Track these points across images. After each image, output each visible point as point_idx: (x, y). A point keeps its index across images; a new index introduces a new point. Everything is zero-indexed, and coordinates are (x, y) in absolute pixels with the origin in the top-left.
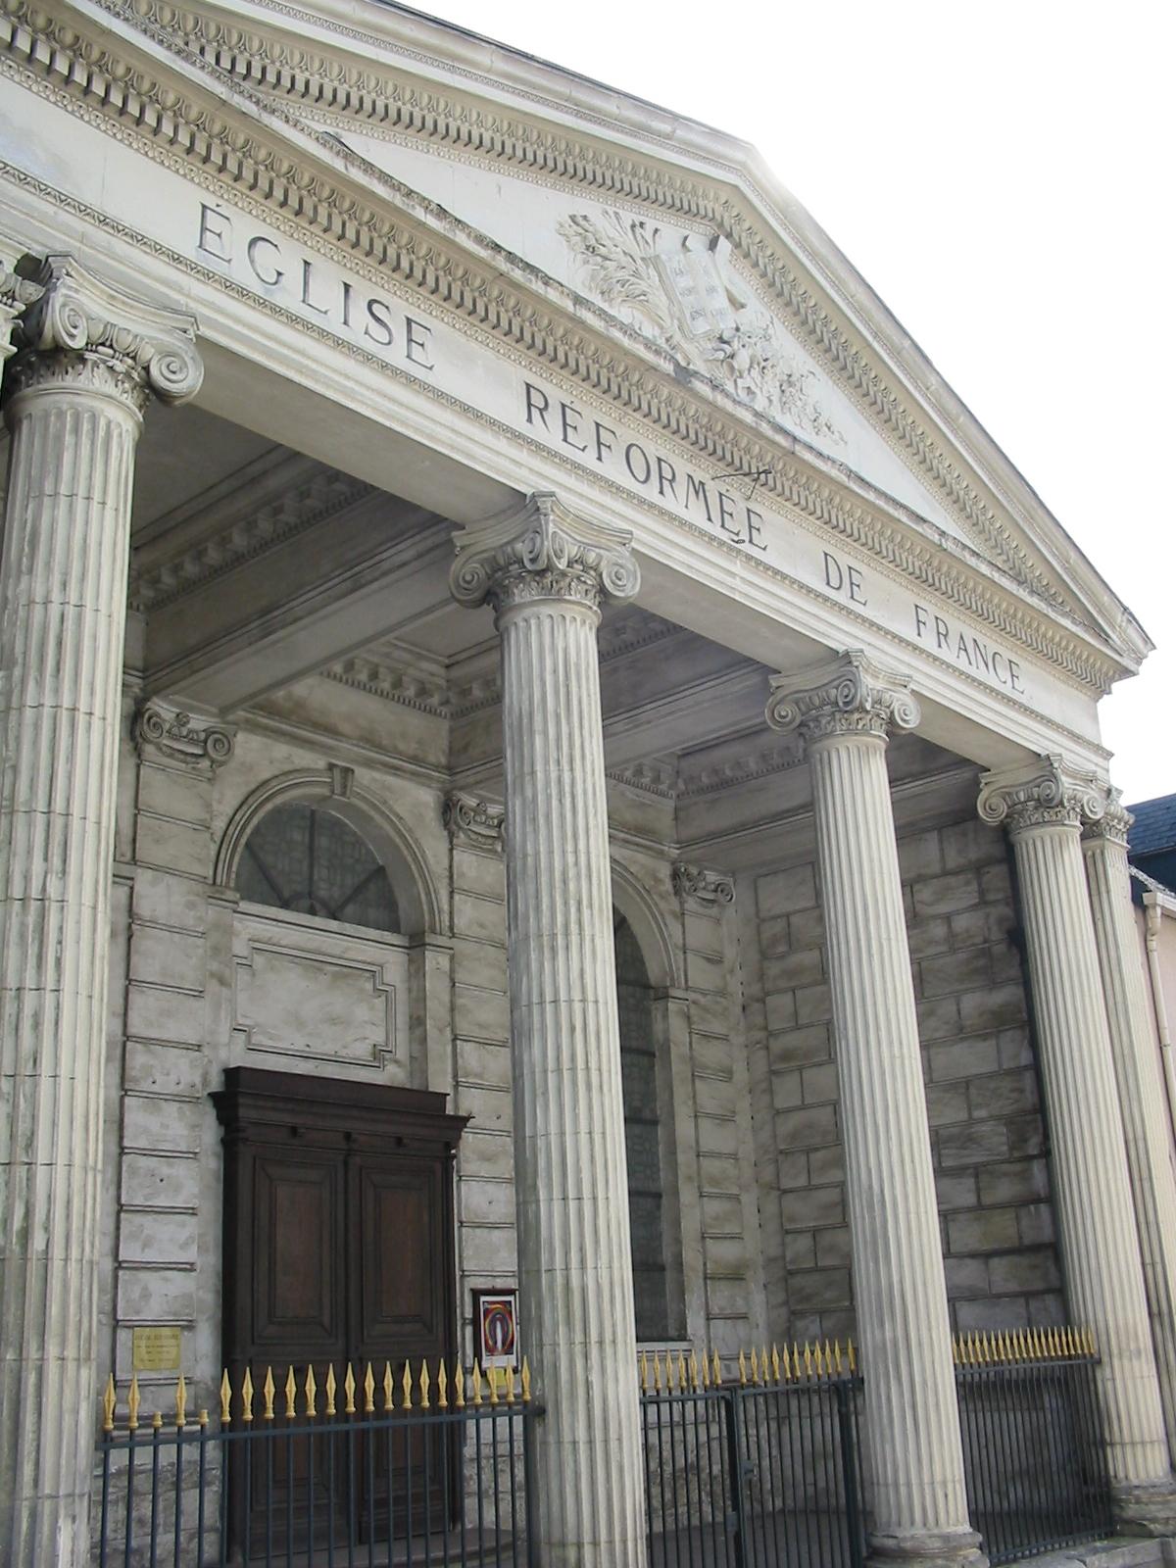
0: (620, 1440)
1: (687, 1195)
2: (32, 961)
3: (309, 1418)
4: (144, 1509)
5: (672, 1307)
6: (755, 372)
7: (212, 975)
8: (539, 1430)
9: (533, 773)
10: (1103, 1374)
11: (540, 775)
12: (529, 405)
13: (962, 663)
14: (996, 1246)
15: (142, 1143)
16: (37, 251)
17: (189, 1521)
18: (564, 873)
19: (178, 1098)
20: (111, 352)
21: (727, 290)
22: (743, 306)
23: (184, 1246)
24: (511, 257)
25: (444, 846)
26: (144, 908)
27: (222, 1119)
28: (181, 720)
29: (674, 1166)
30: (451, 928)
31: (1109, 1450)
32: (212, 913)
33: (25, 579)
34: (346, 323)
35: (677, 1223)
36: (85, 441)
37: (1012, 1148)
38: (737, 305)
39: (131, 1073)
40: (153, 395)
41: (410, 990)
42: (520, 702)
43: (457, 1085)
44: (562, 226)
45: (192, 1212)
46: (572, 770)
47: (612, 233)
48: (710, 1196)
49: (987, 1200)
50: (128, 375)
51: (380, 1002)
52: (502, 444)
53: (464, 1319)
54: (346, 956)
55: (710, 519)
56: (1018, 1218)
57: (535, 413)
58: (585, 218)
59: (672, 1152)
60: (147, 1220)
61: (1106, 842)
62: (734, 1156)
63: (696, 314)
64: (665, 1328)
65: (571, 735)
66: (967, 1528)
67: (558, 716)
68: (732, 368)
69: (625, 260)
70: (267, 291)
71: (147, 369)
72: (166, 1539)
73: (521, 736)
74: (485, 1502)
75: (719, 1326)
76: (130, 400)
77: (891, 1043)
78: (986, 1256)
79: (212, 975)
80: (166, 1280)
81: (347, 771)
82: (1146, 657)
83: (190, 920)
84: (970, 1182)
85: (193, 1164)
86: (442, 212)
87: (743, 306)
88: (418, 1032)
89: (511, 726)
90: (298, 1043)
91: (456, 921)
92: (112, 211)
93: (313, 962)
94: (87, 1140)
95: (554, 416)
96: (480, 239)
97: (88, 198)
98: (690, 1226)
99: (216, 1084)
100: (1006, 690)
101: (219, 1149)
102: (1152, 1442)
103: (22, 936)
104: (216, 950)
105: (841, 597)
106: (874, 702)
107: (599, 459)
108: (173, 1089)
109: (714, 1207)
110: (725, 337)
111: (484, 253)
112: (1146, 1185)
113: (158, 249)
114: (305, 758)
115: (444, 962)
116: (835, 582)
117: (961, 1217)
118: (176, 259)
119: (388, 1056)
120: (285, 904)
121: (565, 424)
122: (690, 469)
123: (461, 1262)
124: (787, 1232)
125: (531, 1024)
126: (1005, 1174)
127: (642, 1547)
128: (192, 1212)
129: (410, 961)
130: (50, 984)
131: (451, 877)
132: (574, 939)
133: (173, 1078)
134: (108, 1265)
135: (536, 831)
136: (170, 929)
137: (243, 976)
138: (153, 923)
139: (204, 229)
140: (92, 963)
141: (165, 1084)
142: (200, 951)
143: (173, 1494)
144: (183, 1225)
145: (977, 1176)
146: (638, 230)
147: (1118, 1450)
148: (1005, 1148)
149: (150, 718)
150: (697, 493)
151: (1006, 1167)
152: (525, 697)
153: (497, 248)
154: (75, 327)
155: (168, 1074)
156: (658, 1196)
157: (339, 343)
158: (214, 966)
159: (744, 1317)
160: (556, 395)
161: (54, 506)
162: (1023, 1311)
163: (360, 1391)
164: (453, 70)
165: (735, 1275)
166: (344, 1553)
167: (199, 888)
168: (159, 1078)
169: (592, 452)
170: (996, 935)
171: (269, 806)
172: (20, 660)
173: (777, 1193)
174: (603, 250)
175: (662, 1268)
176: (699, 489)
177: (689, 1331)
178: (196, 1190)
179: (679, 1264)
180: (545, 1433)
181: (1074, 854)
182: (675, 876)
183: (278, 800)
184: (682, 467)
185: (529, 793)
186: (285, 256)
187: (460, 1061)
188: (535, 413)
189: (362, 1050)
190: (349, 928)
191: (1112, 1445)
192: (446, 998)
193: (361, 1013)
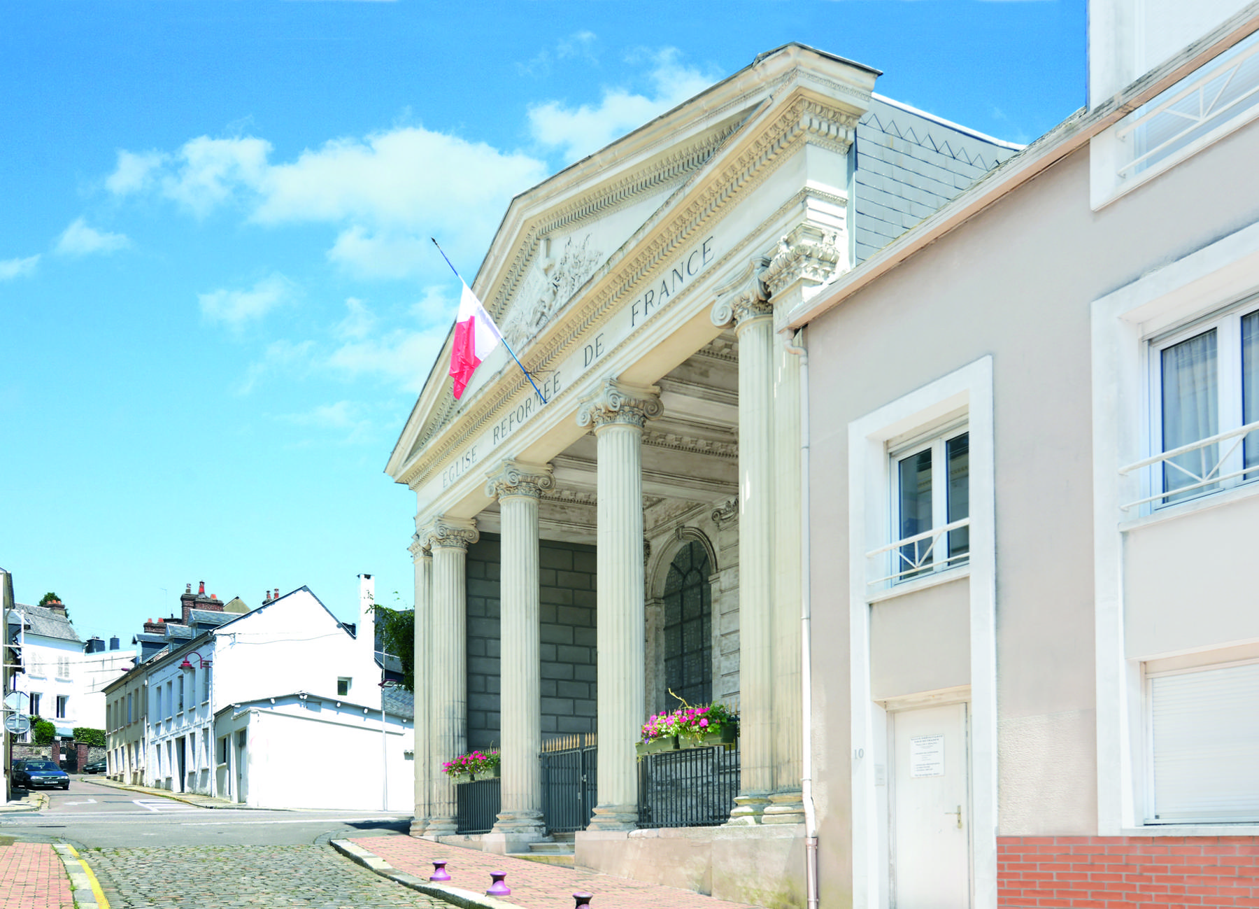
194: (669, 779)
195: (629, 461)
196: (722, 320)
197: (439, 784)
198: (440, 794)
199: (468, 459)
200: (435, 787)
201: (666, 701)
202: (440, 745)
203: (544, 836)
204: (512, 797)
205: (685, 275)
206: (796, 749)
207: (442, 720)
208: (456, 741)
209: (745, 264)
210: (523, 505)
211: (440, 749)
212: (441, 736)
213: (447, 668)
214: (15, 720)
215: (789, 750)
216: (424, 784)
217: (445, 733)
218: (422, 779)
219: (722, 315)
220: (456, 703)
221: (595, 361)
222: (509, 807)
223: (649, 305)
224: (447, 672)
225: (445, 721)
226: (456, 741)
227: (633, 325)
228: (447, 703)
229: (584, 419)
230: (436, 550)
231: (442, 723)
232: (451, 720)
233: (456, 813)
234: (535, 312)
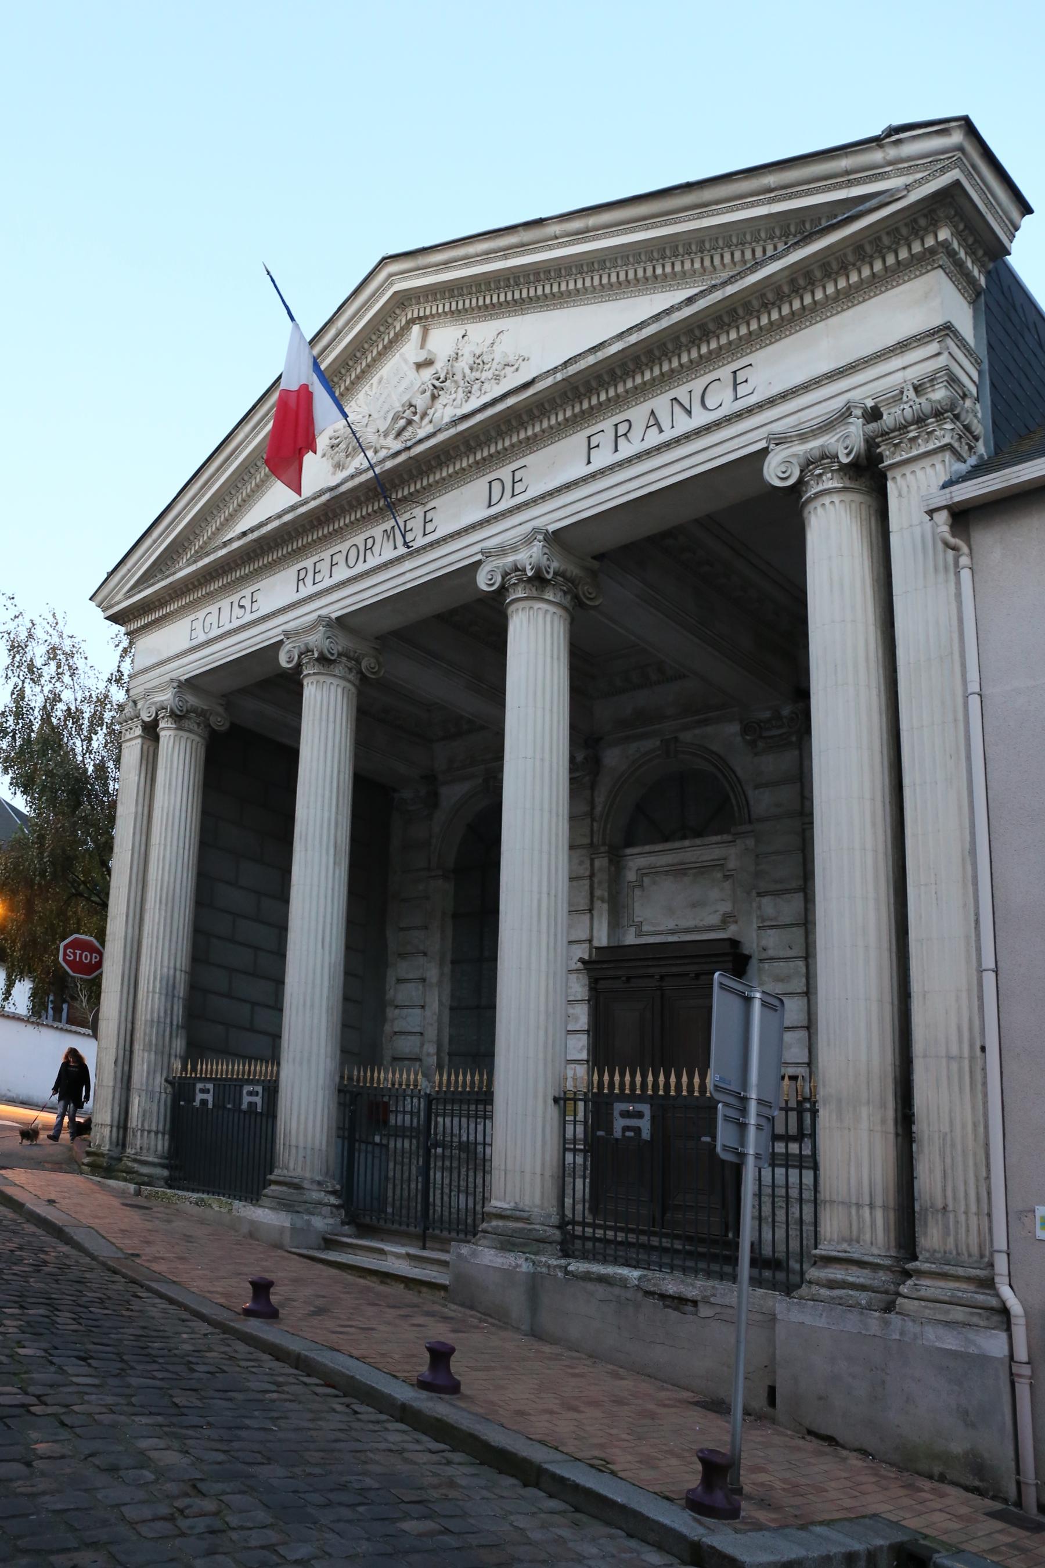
3: (604, 1094)
20: (829, 460)
51: (727, 885)
54: (700, 860)
74: (764, 1226)
90: (671, 924)
91: (137, 778)
93: (679, 871)
120: (666, 840)
124: (569, 1032)
193: (714, 894)
194: (456, 1139)
195: (558, 658)
196: (782, 479)
197: (143, 1099)
198: (144, 1115)
199: (242, 607)
200: (136, 1102)
201: (450, 1022)
202: (151, 1035)
203: (343, 1223)
204: (297, 1153)
205: (696, 408)
206: (962, 1195)
207: (157, 996)
208: (174, 1034)
209: (838, 404)
210: (340, 690)
211: (150, 1041)
212: (152, 1021)
213: (169, 914)
214: (483, 1213)
215: (944, 1190)
216: (114, 1092)
217: (159, 1017)
218: (111, 1084)
219: (784, 472)
220: (178, 973)
221: (507, 503)
222: (291, 1166)
223: (301, 583)
224: (169, 921)
225: (160, 999)
226: (174, 1034)
227: (643, 440)
228: (165, 970)
229: (491, 580)
230: (167, 733)
231: (157, 1000)
232: (170, 998)
233: (166, 1148)
234: (396, 418)
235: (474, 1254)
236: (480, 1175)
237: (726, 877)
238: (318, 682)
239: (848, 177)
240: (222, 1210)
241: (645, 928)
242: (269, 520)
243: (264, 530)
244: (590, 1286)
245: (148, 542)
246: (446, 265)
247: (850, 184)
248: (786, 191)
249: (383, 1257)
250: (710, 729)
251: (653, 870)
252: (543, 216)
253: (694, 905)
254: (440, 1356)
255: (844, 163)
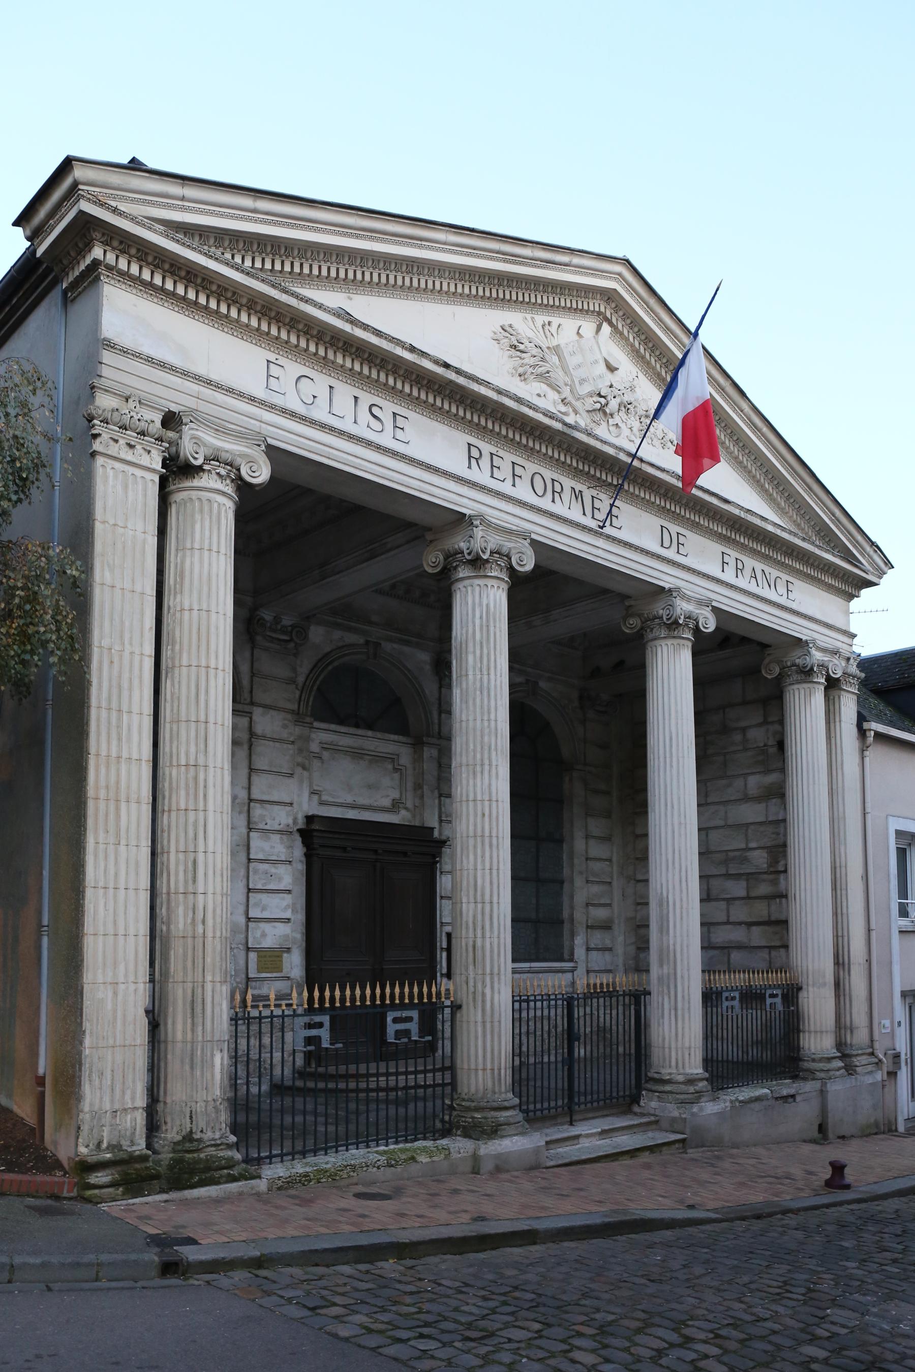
0: (500, 1022)
1: (579, 882)
2: (192, 797)
4: (266, 1040)
5: (567, 943)
6: (622, 414)
7: (298, 764)
8: (458, 1015)
9: (467, 675)
10: (802, 995)
11: (471, 677)
12: (470, 457)
13: (752, 587)
14: (755, 920)
15: (261, 856)
16: (174, 408)
17: (288, 1047)
18: (482, 731)
19: (280, 832)
21: (605, 360)
22: (617, 369)
23: (286, 908)
24: (458, 372)
25: (435, 687)
26: (258, 729)
27: (304, 843)
28: (277, 620)
29: (572, 865)
30: (439, 733)
31: (801, 1034)
32: (298, 730)
33: (179, 596)
34: (355, 422)
35: (572, 897)
36: (207, 517)
37: (770, 866)
38: (611, 369)
39: (254, 819)
40: (243, 487)
41: (414, 769)
42: (462, 634)
43: (441, 821)
44: (495, 333)
45: (289, 892)
46: (489, 674)
47: (531, 334)
48: (593, 882)
49: (752, 894)
50: (228, 476)
51: (396, 776)
52: (452, 485)
53: (442, 949)
55: (584, 514)
56: (769, 905)
57: (473, 461)
58: (511, 326)
59: (571, 857)
60: (264, 897)
61: (843, 693)
62: (610, 860)
63: (582, 381)
64: (562, 954)
65: (488, 654)
66: (700, 1071)
67: (481, 643)
68: (605, 413)
69: (535, 351)
70: (307, 409)
71: (239, 470)
72: (277, 1055)
73: (461, 654)
75: (594, 954)
76: (230, 489)
77: (680, 815)
78: (750, 924)
79: (298, 764)
80: (275, 927)
81: (377, 645)
82: (885, 573)
83: (285, 735)
84: (743, 884)
85: (289, 867)
86: (412, 349)
87: (617, 369)
88: (419, 792)
89: (456, 648)
92: (214, 377)
93: (357, 754)
94: (222, 881)
95: (485, 462)
96: (437, 362)
97: (201, 371)
98: (580, 898)
99: (301, 824)
100: (782, 601)
101: (304, 859)
102: (822, 1032)
103: (187, 785)
104: (300, 751)
105: (671, 554)
106: (685, 618)
107: (514, 485)
108: (277, 827)
109: (595, 889)
110: (602, 394)
111: (440, 370)
112: (844, 892)
113: (241, 395)
114: (353, 638)
115: (435, 752)
116: (666, 544)
117: (737, 902)
118: (252, 400)
119: (401, 805)
121: (492, 466)
122: (573, 483)
123: (441, 918)
125: (462, 812)
126: (764, 881)
127: (509, 1072)
128: (289, 892)
129: (415, 752)
130: (201, 807)
131: (440, 704)
132: (487, 767)
133: (277, 821)
134: (242, 920)
135: (467, 708)
136: (274, 740)
137: (316, 763)
138: (264, 737)
139: (269, 376)
140: (222, 796)
141: (273, 825)
142: (291, 752)
143: (280, 1034)
144: (283, 899)
145: (747, 880)
146: (547, 327)
147: (807, 1034)
148: (765, 866)
149: (259, 620)
150: (577, 498)
151: (765, 876)
152: (464, 631)
153: (447, 366)
154: (197, 453)
155: (274, 820)
156: (562, 882)
157: (351, 437)
158: (299, 759)
159: (610, 949)
160: (487, 448)
161: (192, 556)
162: (767, 957)
163: (363, 997)
164: (420, 247)
165: (606, 926)
166: (279, 1099)
167: (289, 716)
168: (269, 821)
169: (509, 481)
170: (771, 742)
171: (330, 668)
172: (178, 641)
173: (632, 882)
174: (522, 347)
175: (562, 922)
176: (578, 495)
177: (576, 957)
178: (290, 881)
179: (572, 920)
180: (462, 1016)
181: (818, 698)
182: (581, 698)
183: (336, 664)
184: (568, 483)
185: (464, 686)
186: (321, 382)
187: (443, 809)
188: (473, 461)
189: (386, 802)
190: (379, 735)
191: (804, 1032)
192: (435, 773)
193: (386, 781)
235: (701, 1109)
236: (709, 1056)
237: (396, 770)
238: (499, 587)
239: (856, 543)
240: (435, 1159)
241: (324, 798)
242: (487, 384)
243: (475, 387)
244: (752, 1105)
245: (246, 202)
246: (667, 329)
247: (854, 546)
248: (837, 521)
249: (576, 1142)
250: (406, 649)
251: (332, 747)
252: (748, 395)
253: (369, 787)
254: (838, 1169)
255: (859, 538)
